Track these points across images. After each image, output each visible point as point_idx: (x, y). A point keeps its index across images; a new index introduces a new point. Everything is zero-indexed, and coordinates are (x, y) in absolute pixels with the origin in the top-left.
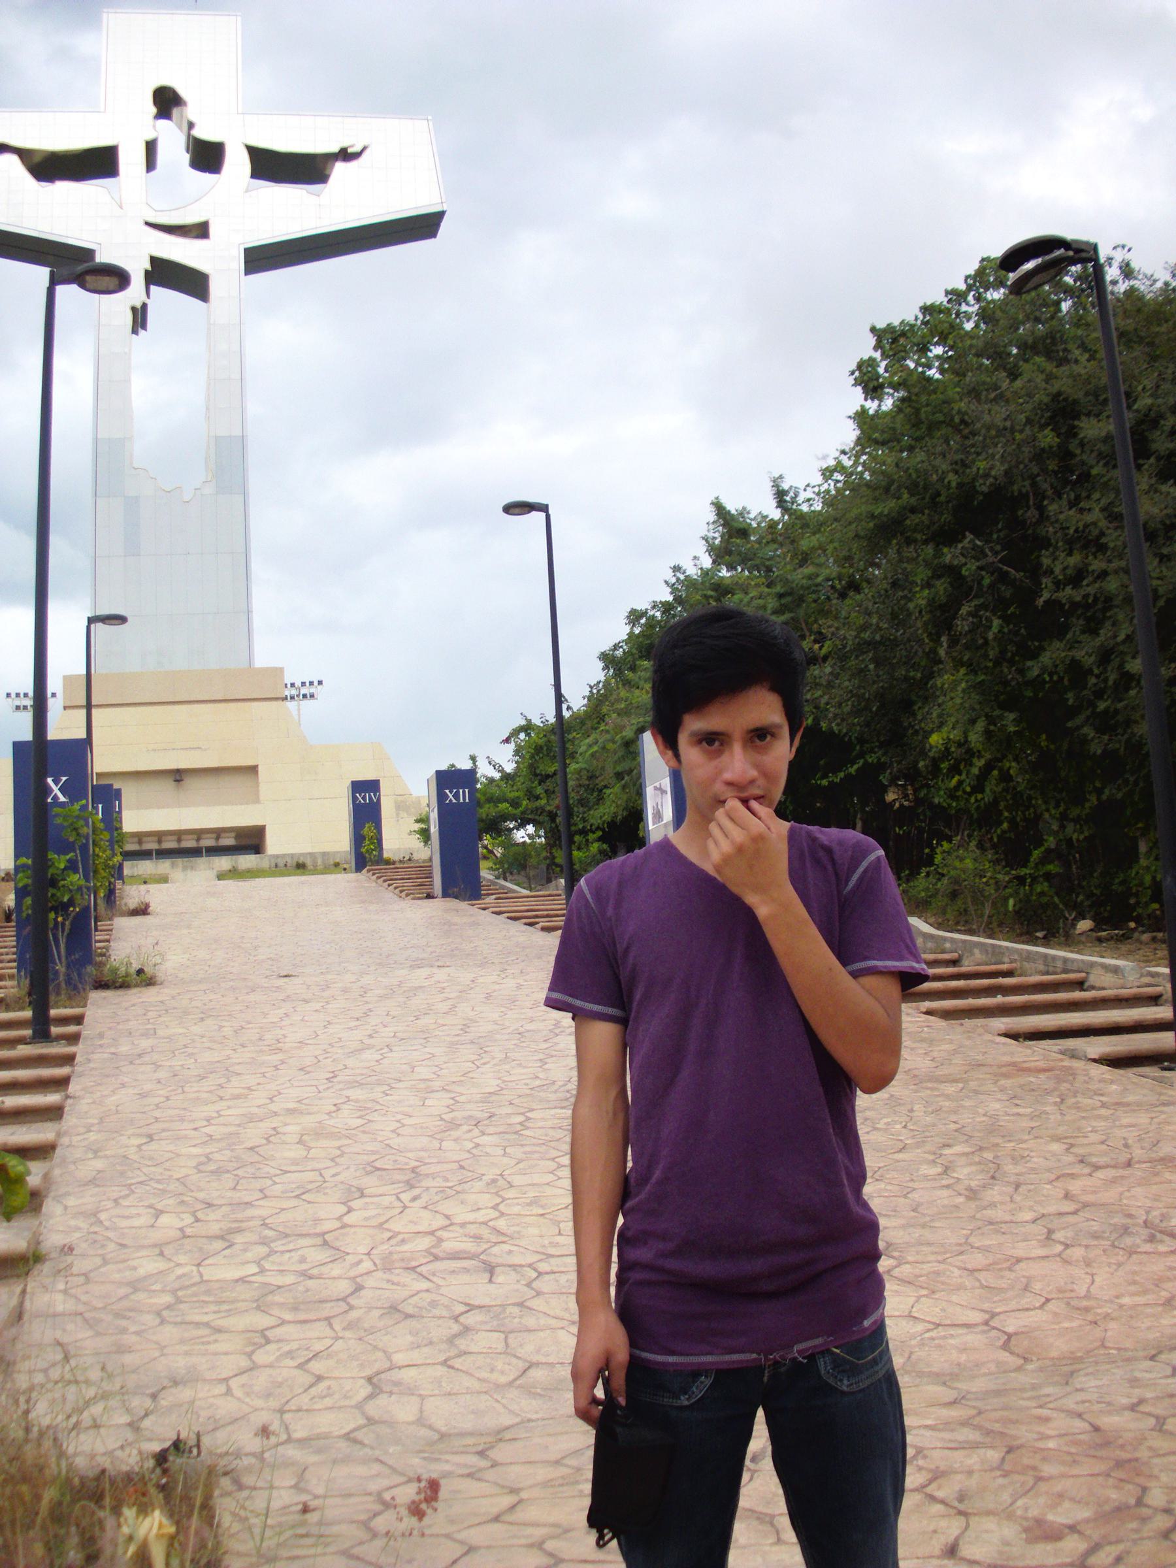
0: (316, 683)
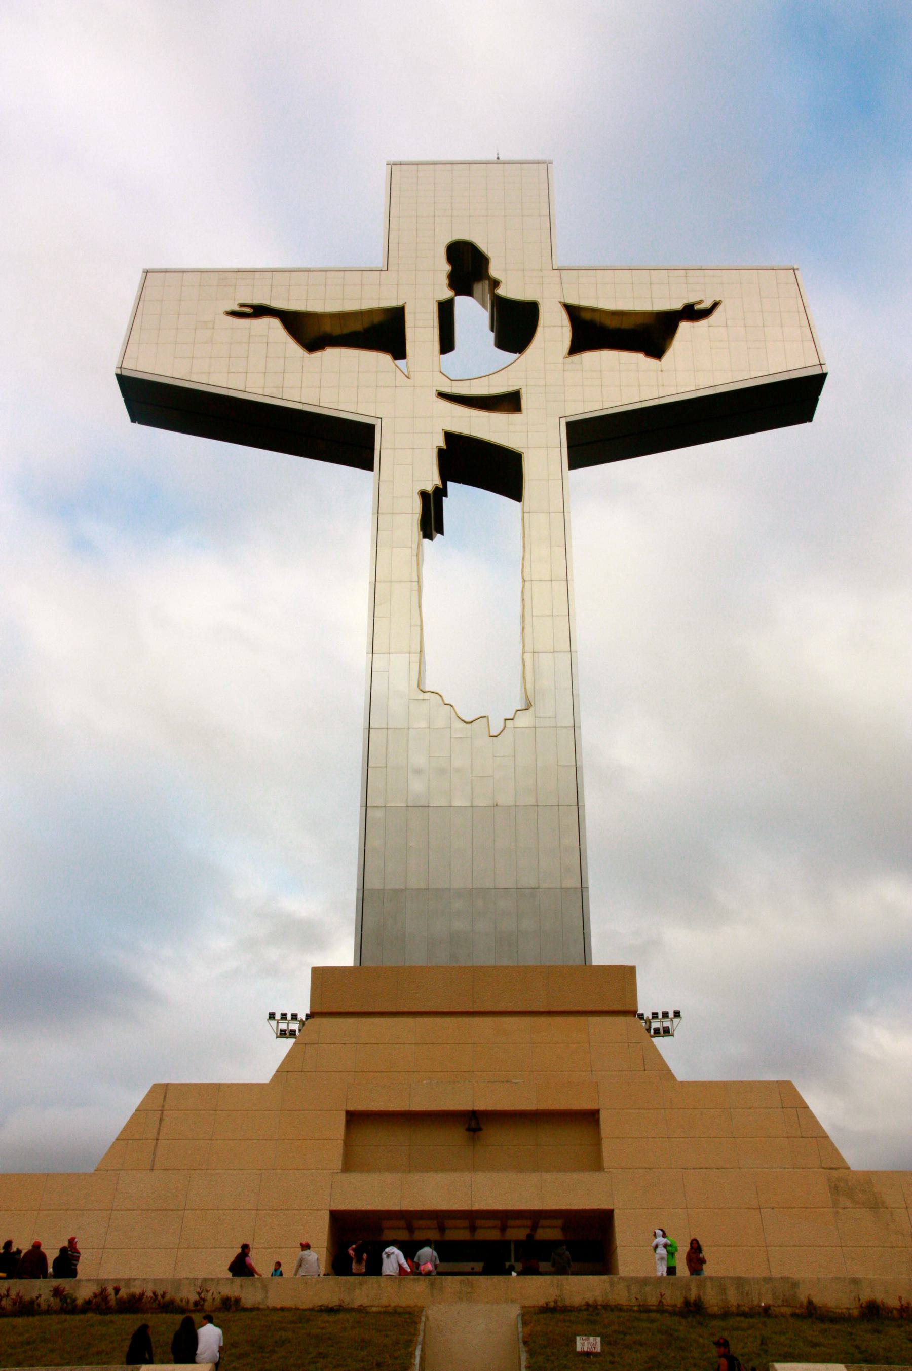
0: (671, 1015)
